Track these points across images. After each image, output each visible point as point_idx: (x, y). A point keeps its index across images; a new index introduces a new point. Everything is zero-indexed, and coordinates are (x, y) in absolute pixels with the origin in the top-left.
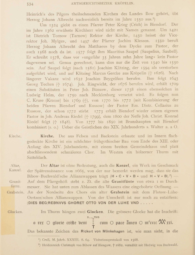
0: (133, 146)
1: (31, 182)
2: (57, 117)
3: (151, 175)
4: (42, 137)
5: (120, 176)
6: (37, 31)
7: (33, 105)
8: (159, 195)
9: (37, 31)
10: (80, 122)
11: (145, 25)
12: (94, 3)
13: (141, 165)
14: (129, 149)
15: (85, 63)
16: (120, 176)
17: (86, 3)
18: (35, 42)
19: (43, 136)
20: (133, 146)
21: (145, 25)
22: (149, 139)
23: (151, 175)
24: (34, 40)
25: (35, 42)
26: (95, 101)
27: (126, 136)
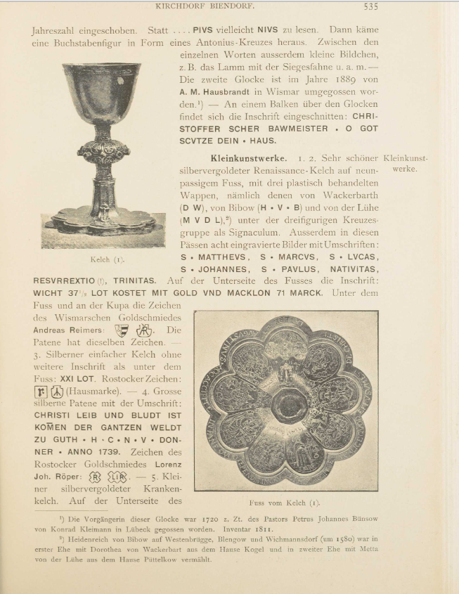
0: (89, 463)
1: (174, 281)
2: (232, 106)
3: (94, 438)
4: (214, 162)
5: (111, 440)
6: (317, 68)
7: (100, 462)
8: (99, 556)
9: (317, 68)
10: (237, 56)
11: (257, 93)
12: (180, 6)
13: (58, 316)
14: (254, 525)
15: (265, 117)
16: (111, 440)
17: (62, 549)
18: (215, 43)
19: (217, 159)
20: (89, 463)
21: (257, 93)
22: (124, 410)
23: (94, 438)
24: (212, 41)
25: (215, 43)
26: (308, 196)
27: (359, 196)
